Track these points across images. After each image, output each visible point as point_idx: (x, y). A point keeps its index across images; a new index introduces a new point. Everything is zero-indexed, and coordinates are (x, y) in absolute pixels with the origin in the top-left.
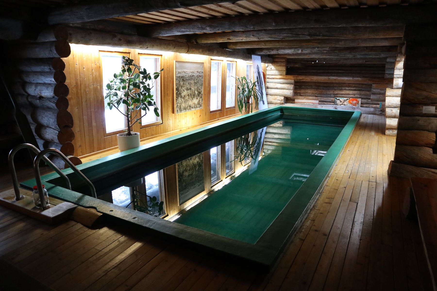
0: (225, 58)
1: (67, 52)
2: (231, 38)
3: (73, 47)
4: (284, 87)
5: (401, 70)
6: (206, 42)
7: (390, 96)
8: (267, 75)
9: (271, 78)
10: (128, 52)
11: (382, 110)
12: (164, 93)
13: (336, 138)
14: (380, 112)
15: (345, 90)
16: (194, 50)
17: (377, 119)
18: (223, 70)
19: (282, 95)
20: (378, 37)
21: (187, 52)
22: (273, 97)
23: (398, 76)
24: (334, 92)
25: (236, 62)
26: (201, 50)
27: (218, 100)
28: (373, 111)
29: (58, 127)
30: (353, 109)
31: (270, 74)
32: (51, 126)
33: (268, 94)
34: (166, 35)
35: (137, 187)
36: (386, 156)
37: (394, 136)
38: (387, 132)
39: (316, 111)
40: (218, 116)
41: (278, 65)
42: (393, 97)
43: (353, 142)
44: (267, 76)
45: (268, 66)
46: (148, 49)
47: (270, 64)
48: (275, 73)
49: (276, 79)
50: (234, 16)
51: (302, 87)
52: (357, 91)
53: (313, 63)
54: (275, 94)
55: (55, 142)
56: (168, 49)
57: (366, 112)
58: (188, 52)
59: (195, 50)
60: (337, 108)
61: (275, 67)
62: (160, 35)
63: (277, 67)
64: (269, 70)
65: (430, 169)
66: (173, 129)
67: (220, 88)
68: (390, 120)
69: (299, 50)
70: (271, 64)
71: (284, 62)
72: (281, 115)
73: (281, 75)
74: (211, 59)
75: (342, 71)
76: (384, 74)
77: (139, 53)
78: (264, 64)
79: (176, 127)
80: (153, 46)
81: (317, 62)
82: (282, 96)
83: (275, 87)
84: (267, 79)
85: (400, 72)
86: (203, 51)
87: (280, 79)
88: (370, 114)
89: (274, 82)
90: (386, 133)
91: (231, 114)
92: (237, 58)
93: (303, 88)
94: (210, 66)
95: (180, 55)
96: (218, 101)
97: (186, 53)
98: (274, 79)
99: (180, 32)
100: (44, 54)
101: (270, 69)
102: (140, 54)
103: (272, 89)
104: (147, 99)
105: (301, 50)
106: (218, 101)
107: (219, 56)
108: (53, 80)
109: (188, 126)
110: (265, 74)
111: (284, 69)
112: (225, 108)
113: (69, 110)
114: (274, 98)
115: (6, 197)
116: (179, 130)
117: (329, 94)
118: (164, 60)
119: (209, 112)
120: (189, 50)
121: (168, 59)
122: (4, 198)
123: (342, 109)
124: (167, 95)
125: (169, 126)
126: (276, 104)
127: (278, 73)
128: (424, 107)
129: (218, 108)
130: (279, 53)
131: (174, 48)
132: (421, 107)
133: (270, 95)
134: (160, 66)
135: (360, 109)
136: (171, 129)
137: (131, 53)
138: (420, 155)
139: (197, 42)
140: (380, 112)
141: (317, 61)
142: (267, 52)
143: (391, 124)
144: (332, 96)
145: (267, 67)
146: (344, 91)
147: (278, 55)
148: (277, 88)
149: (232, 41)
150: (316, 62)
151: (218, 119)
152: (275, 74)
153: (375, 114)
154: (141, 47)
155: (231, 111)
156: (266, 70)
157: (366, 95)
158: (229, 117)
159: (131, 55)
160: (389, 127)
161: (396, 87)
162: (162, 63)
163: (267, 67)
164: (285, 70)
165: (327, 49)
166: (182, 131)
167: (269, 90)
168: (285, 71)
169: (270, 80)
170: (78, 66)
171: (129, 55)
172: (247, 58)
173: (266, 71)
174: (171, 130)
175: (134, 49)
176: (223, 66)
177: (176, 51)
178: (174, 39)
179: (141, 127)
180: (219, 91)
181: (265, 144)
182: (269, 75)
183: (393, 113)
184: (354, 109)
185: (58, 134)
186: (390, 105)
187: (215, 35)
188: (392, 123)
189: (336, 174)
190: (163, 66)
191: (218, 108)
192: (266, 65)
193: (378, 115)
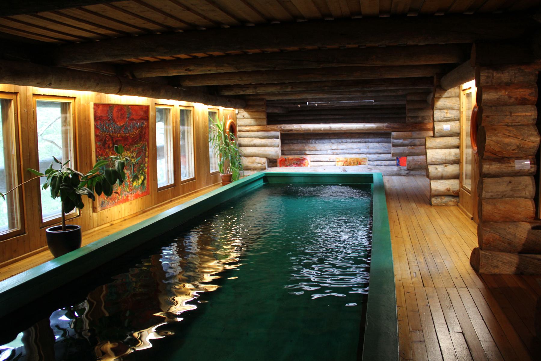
0: (177, 101)
2: (191, 68)
4: (265, 143)
5: (442, 110)
6: (149, 75)
7: (432, 148)
8: (239, 126)
9: (244, 130)
10: (13, 91)
11: (409, 168)
12: (81, 163)
14: (406, 172)
15: (347, 142)
16: (129, 89)
17: (407, 182)
18: (174, 121)
19: (263, 155)
20: (417, 63)
21: (118, 92)
22: (250, 159)
23: (439, 119)
24: (331, 146)
27: (168, 167)
28: (397, 171)
30: (369, 169)
31: (242, 125)
34: (84, 63)
36: (453, 239)
37: (444, 206)
38: (434, 201)
39: (329, 177)
40: (170, 195)
42: (436, 148)
43: (394, 222)
44: (238, 128)
45: (238, 112)
46: (52, 86)
47: (242, 110)
48: (251, 123)
49: (252, 131)
51: (285, 142)
52: (362, 143)
53: (299, 106)
54: (252, 154)
56: (87, 86)
57: (388, 173)
59: (130, 89)
60: (346, 170)
61: (249, 114)
62: (74, 62)
63: (253, 113)
64: (241, 119)
65: (533, 256)
66: (98, 225)
67: (170, 150)
68: (436, 183)
70: (242, 109)
71: (262, 105)
73: (259, 125)
74: (156, 104)
75: (340, 117)
76: (405, 118)
77: (34, 95)
78: (234, 109)
79: (103, 220)
80: (60, 81)
81: (308, 104)
82: (263, 156)
83: (252, 143)
84: (239, 132)
85: (442, 113)
86: (143, 91)
87: (258, 131)
88: (393, 175)
89: (249, 136)
90: (432, 202)
91: (189, 190)
92: (195, 101)
93: (286, 143)
94: (154, 115)
95: (105, 97)
98: (248, 131)
101: (242, 117)
102: (37, 96)
103: (246, 148)
105: (290, 87)
106: (168, 171)
107: (168, 99)
109: (123, 216)
110: (235, 124)
111: (264, 116)
112: (180, 182)
114: (251, 161)
116: (109, 224)
117: (325, 149)
118: (79, 105)
119: (156, 190)
120: (122, 89)
121: (86, 104)
123: (353, 170)
124: (86, 165)
125: (92, 219)
126: (254, 169)
127: (255, 122)
128: (515, 161)
129: (168, 183)
130: (259, 92)
131: (97, 84)
132: (512, 163)
134: (73, 116)
135: (379, 170)
136: (96, 224)
137: (19, 94)
138: (518, 236)
139: (133, 76)
140: (406, 172)
141: (308, 103)
142: (240, 91)
143: (438, 188)
144: (329, 152)
145: (238, 114)
146: (345, 144)
147: (257, 94)
148: (255, 146)
149: (193, 74)
150: (306, 105)
151: (170, 200)
152: (251, 124)
153: (399, 175)
154: (38, 83)
156: (236, 118)
157: (376, 148)
158: (187, 195)
159: (20, 98)
160: (436, 193)
161: (438, 134)
162: (75, 111)
163: (238, 114)
164: (265, 117)
166: (115, 225)
167: (243, 148)
168: (264, 119)
171: (15, 96)
172: (209, 101)
174: (94, 227)
175: (25, 87)
176: (174, 113)
177: (101, 90)
178: (95, 70)
179: (41, 226)
180: (169, 154)
182: (241, 126)
183: (439, 172)
184: (371, 170)
186: (433, 162)
187: (163, 64)
188: (439, 187)
189: (400, 281)
190: (78, 116)
191: (168, 183)
192: (236, 111)
193: (404, 176)
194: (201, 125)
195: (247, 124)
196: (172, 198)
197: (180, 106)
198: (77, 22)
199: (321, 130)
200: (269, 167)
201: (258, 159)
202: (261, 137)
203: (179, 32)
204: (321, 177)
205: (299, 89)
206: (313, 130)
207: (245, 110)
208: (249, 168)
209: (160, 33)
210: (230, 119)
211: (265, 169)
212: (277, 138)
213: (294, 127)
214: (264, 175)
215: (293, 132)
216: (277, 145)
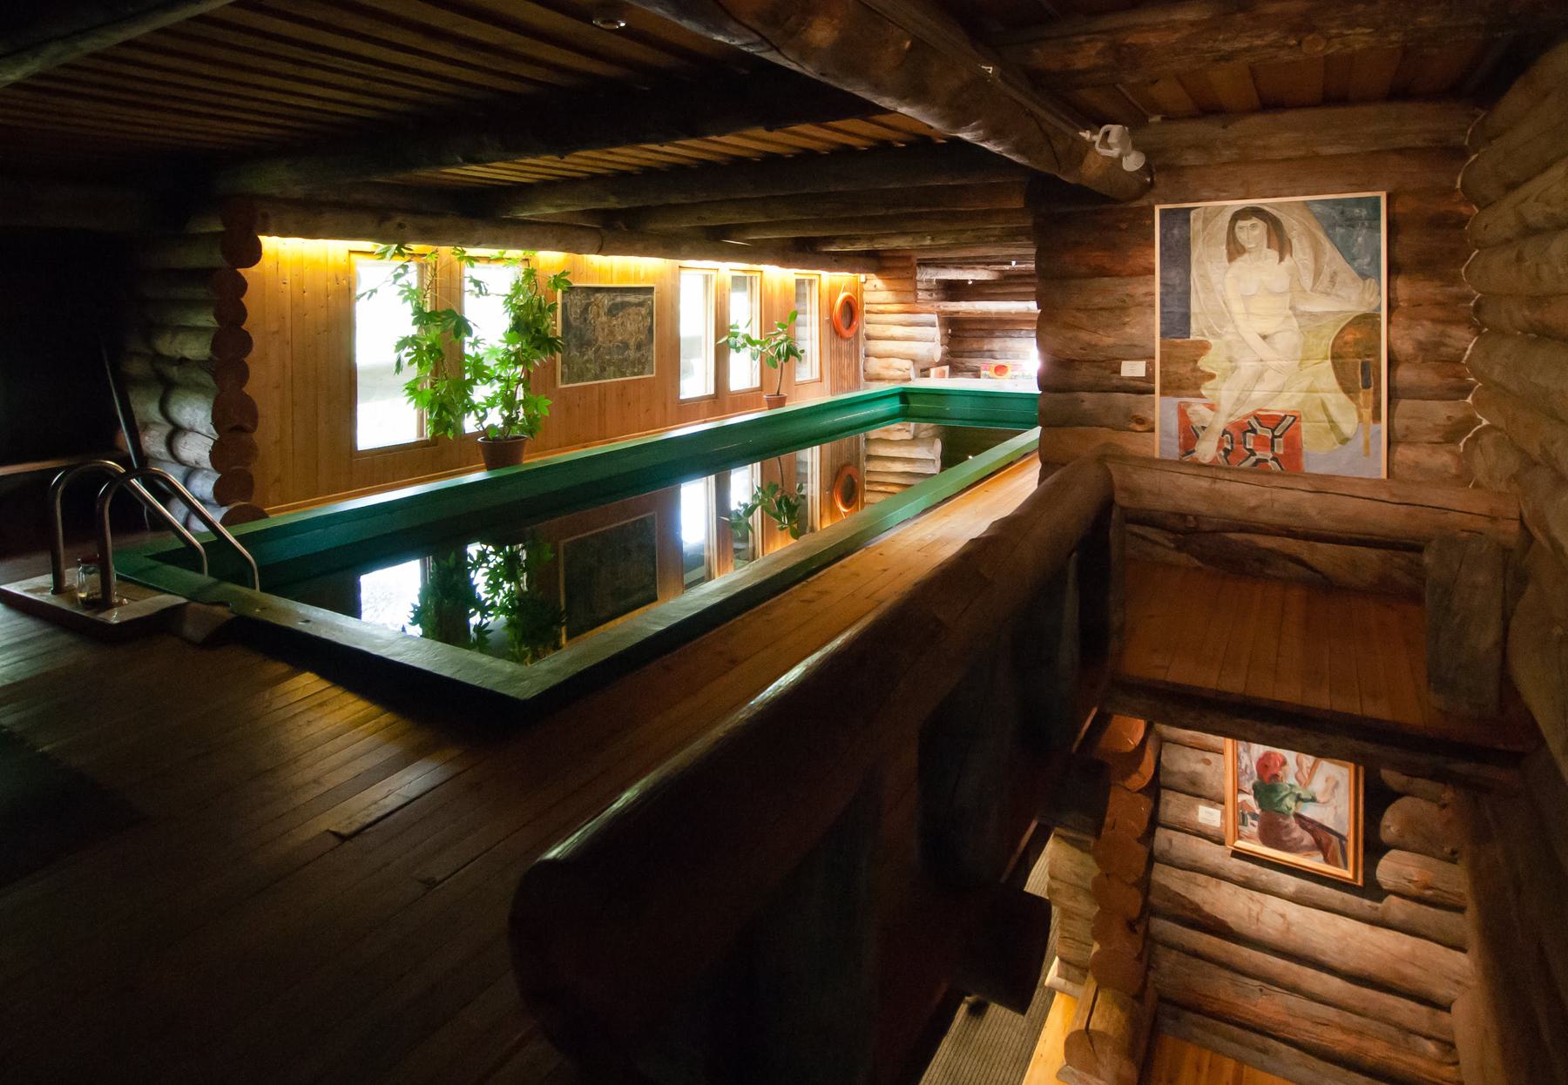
1: (254, 254)
3: (270, 244)
9: (876, 311)
13: (961, 462)
22: (883, 362)
25: (761, 272)
26: (639, 246)
29: (214, 432)
32: (199, 430)
33: (870, 353)
35: (1079, 749)
41: (893, 277)
44: (866, 308)
45: (866, 280)
47: (872, 276)
50: (790, 156)
55: (203, 469)
58: (601, 250)
69: (924, 237)
70: (873, 275)
72: (900, 407)
74: (680, 267)
96: (706, 374)
97: (597, 254)
99: (552, 206)
100: (197, 258)
101: (873, 288)
104: (654, 375)
105: (929, 237)
106: (706, 374)
108: (212, 318)
113: (248, 389)
115: (34, 588)
122: (25, 591)
126: (891, 380)
131: (559, 242)
133: (876, 357)
145: (865, 283)
155: (744, 400)
165: (996, 233)
167: (872, 343)
169: (874, 317)
170: (289, 287)
173: (861, 296)
181: (868, 491)
185: (213, 447)
192: (862, 277)
194: (777, 302)
195: (881, 300)
196: (708, 417)
197: (731, 270)
198: (847, 137)
199: (990, 313)
200: (916, 376)
201: (897, 363)
202: (904, 323)
203: (899, 148)
204: (350, 413)
205: (944, 242)
206: (996, 313)
207: (877, 275)
208: (881, 376)
209: (903, 145)
210: (845, 290)
211: (910, 379)
212: (933, 325)
213: (961, 306)
214: (900, 391)
215: (960, 315)
216: (931, 339)
